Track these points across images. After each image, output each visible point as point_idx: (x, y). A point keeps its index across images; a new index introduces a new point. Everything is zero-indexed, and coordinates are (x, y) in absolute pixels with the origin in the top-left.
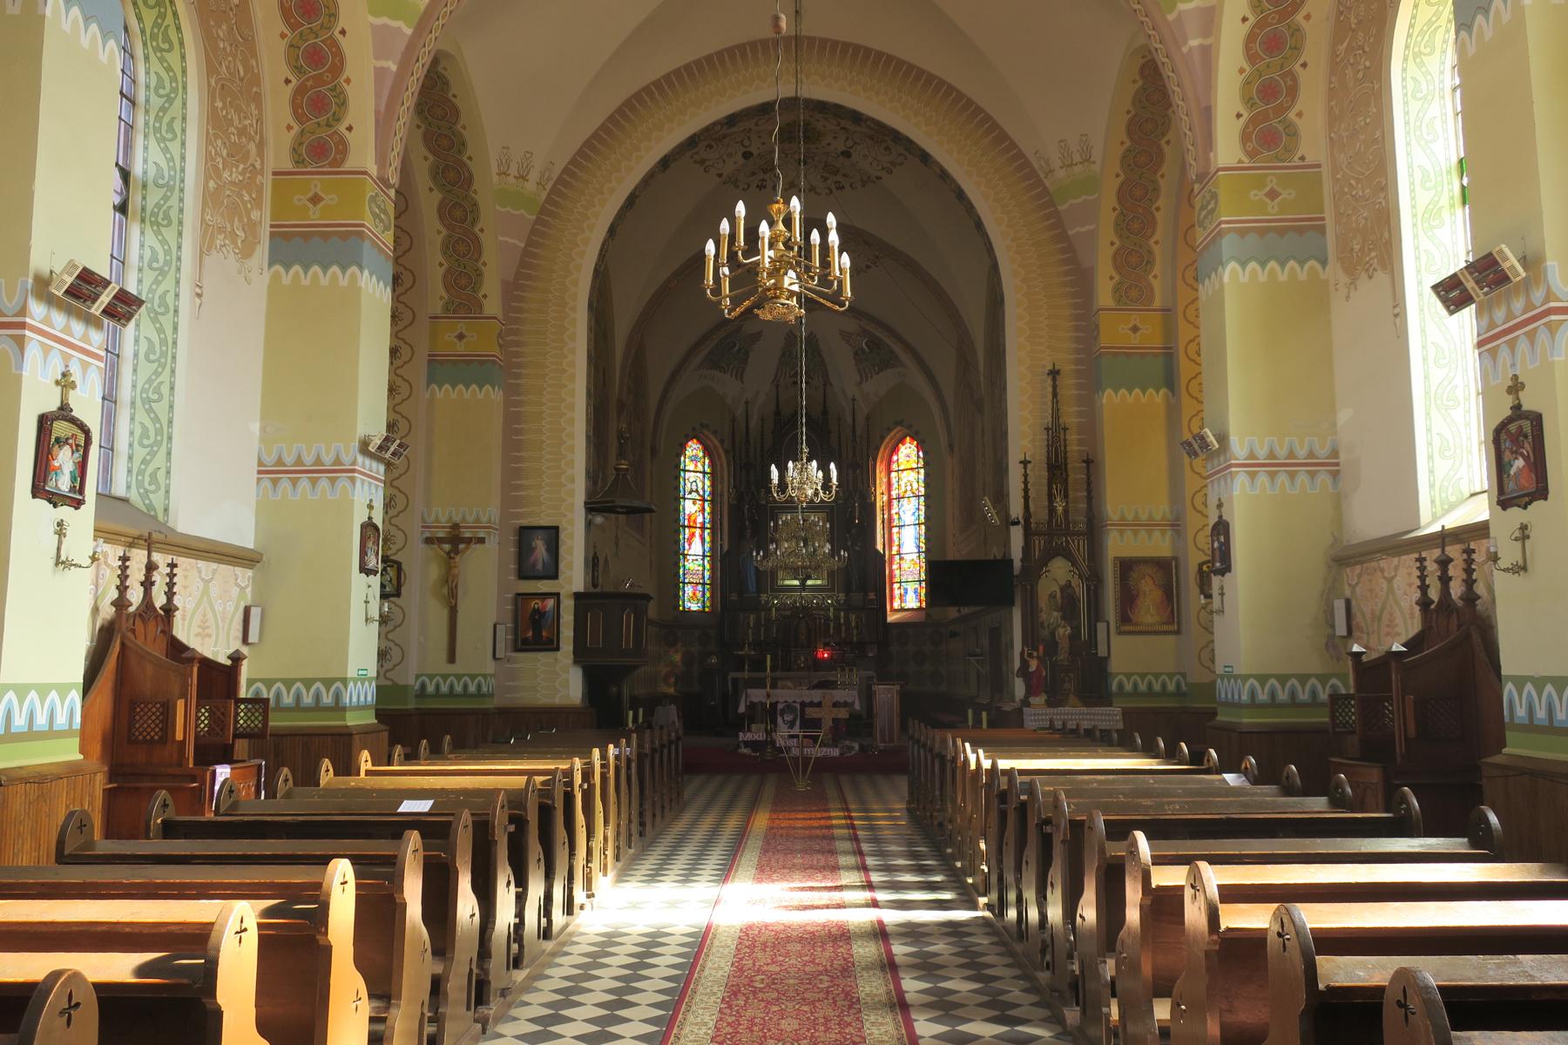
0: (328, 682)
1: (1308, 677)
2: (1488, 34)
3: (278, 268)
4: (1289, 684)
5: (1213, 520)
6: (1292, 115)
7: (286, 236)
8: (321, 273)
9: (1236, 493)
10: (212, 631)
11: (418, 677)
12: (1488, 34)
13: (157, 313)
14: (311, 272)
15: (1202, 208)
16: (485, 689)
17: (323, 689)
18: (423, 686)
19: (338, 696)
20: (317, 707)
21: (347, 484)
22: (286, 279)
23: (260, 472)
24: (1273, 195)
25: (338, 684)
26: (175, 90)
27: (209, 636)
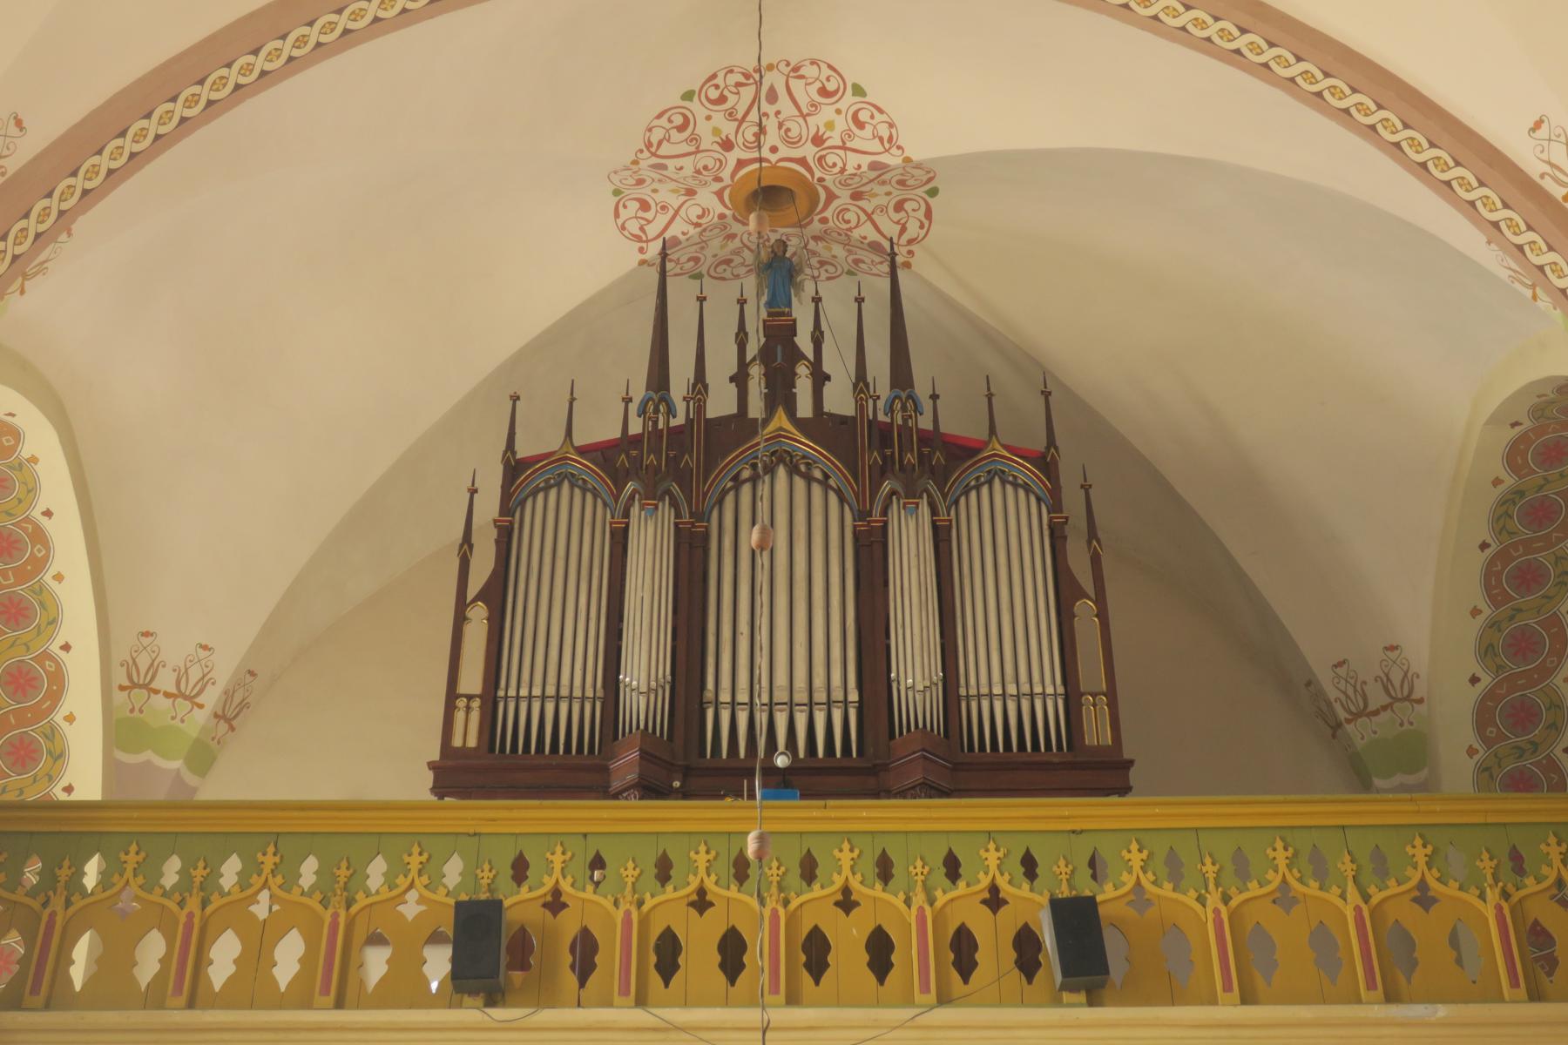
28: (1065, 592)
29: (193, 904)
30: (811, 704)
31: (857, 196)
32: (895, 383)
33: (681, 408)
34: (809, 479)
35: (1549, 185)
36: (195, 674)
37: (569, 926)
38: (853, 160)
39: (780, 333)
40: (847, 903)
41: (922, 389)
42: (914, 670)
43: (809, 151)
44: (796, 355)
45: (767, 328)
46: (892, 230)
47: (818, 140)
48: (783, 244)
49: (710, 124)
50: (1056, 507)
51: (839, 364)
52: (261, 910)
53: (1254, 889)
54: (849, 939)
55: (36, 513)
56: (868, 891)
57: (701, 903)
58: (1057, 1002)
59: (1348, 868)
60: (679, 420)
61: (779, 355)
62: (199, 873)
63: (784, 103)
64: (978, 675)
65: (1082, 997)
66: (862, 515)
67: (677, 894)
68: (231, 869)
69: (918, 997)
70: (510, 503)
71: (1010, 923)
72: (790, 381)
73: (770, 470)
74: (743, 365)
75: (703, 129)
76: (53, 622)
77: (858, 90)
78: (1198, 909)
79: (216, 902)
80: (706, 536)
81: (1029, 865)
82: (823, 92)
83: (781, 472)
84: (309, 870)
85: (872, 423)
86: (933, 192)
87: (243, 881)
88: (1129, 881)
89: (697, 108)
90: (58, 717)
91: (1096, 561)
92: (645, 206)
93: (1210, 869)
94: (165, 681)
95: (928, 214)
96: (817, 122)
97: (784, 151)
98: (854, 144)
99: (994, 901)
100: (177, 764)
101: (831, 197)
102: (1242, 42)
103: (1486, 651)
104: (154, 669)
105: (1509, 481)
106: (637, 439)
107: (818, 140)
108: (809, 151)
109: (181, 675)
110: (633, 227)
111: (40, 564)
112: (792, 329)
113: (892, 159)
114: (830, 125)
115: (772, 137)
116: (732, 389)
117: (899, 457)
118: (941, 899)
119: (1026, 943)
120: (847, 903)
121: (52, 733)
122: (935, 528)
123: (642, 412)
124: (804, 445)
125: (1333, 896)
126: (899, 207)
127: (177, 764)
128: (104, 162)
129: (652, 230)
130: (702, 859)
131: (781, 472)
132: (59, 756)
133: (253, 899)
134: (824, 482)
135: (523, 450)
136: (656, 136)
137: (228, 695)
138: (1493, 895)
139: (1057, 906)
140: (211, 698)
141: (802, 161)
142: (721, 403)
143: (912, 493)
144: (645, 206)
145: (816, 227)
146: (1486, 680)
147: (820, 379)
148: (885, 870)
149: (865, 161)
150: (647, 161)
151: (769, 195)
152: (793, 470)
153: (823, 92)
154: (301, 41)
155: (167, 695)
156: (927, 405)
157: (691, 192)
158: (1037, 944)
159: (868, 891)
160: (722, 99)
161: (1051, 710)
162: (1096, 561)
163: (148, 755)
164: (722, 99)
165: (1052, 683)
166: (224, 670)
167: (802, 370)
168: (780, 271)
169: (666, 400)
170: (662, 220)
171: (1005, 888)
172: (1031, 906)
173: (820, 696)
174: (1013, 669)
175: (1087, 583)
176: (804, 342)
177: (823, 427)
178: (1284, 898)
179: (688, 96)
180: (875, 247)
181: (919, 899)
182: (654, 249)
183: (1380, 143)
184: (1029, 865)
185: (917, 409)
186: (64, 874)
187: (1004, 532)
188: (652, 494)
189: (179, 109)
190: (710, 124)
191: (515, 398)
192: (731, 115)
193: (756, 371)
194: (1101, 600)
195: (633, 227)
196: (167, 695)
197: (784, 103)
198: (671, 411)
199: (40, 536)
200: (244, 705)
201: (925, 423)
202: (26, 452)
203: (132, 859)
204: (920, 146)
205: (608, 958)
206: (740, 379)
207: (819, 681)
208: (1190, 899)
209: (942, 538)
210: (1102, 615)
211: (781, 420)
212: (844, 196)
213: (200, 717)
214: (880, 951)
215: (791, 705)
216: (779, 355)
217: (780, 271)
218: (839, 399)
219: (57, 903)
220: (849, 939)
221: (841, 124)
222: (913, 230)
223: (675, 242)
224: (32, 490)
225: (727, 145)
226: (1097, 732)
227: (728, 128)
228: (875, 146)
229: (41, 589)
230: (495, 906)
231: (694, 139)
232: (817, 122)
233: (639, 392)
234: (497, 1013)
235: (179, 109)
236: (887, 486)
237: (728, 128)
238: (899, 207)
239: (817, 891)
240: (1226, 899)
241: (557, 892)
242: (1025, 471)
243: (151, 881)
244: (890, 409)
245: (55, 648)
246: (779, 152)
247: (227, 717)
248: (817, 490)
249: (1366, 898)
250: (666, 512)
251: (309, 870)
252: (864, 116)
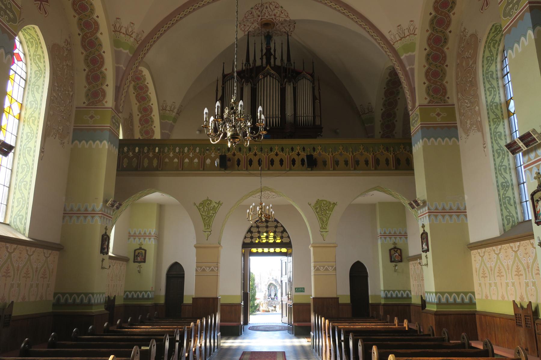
0: (466, 293)
1: (131, 291)
2: (520, 50)
3: (425, 139)
4: (445, 296)
5: (421, 231)
6: (140, 115)
7: (428, 128)
8: (449, 140)
9: (154, 230)
10: (523, 272)
11: (125, 292)
12: (520, 50)
13: (500, 149)
14: (445, 141)
15: (413, 119)
16: (150, 296)
17: (77, 297)
18: (127, 295)
19: (90, 300)
20: (463, 303)
21: (463, 217)
22: (429, 144)
23: (466, 212)
24: (438, 115)
25: (90, 295)
26: (487, 73)
27: (486, 277)
28: (314, 98)
29: (181, 154)
30: (273, 117)
31: (282, 24)
32: (288, 61)
33: (252, 65)
34: (273, 78)
35: (391, 42)
36: (173, 107)
37: (236, 158)
38: (281, 19)
39: (268, 50)
40: (277, 155)
41: (292, 62)
42: (289, 112)
43: (273, 17)
44: (271, 54)
45: (266, 49)
46: (288, 29)
47: (275, 15)
48: (269, 32)
49: (256, 13)
50: (313, 84)
51: (278, 55)
52: (191, 155)
53: (337, 153)
54: (277, 160)
55: (146, 83)
56: (280, 153)
57: (255, 155)
58: (307, 170)
59: (351, 150)
60: (251, 67)
61: (268, 54)
62: (182, 150)
63: (269, 9)
64: (300, 112)
65: (310, 169)
66: (281, 85)
67: (251, 154)
68: (186, 150)
69: (287, 169)
70: (224, 83)
71: (300, 157)
72: (270, 58)
73: (267, 76)
74: (262, 56)
75: (255, 14)
76: (150, 100)
77: (282, 7)
78: (328, 157)
79: (184, 154)
80: (256, 88)
81: (304, 149)
82: (276, 7)
83: (268, 76)
84: (198, 150)
85: (284, 67)
86: (295, 23)
87: (188, 151)
88: (318, 151)
89: (254, 10)
90: (152, 115)
91: (319, 93)
92: (245, 25)
93: (330, 150)
94: (168, 108)
95: (294, 27)
96: (275, 12)
97: (269, 17)
98: (281, 16)
99: (298, 154)
100: (127, 51)
101: (277, 24)
102: (345, 11)
103: (384, 105)
104: (166, 107)
105: (389, 78)
106: (244, 70)
107: (275, 15)
108: (273, 17)
109: (171, 107)
110: (243, 29)
111: (147, 91)
112: (271, 49)
113: (288, 19)
114: (277, 13)
115: (267, 14)
116: (260, 61)
117: (288, 74)
118: (291, 154)
119: (303, 161)
120: (277, 155)
121: (151, 118)
122: (294, 87)
123: (245, 66)
124: (272, 72)
125: (348, 154)
126: (289, 26)
127: (171, 122)
128: (157, 36)
129: (246, 30)
130: (255, 148)
131: (268, 76)
132: (153, 122)
133: (190, 154)
134: (275, 79)
135: (225, 73)
136: (247, 15)
137: (178, 110)
138: (371, 154)
139: (307, 156)
140: (176, 111)
141: (272, 19)
142: (258, 63)
143: (290, 82)
144: (245, 25)
145: (275, 29)
146: (384, 110)
147: (275, 59)
148: (282, 150)
149: (283, 19)
150: (245, 20)
151: (266, 25)
152: (270, 76)
153: (276, 7)
154: (187, 11)
155: (123, 33)
156: (293, 64)
157: (253, 23)
158: (304, 161)
159: (280, 153)
160: (258, 9)
161: (311, 119)
162: (319, 93)
163: (166, 120)
164: (258, 9)
165: (311, 114)
166: (177, 106)
167: (272, 57)
168: (268, 38)
169: (249, 64)
170: (248, 28)
171: (300, 153)
172: (303, 155)
173: (274, 116)
174: (305, 111)
175: (318, 97)
176: (272, 51)
177: (276, 68)
178: (341, 154)
179: (252, 8)
180: (285, 32)
181: (287, 154)
182: (247, 33)
183: (366, 31)
184: (304, 149)
185: (291, 65)
186: (162, 150)
187: (305, 87)
188: (247, 82)
189: (168, 25)
190: (256, 13)
191: (224, 63)
192: (259, 11)
193: (264, 57)
194: (320, 101)
195: (243, 29)
196: (123, 33)
197: (269, 9)
198: (250, 66)
199: (147, 87)
200: (181, 111)
201: (293, 67)
202: (144, 74)
203: (171, 148)
204: (292, 17)
205: (242, 163)
206: (262, 59)
207: (274, 113)
208: (327, 154)
209: (295, 89)
210: (320, 103)
211: (268, 67)
212: (279, 24)
213: (174, 114)
214: (281, 161)
215: (270, 117)
216: (268, 54)
217: (268, 38)
218: (278, 63)
219: (161, 154)
220: (277, 160)
221: (279, 13)
222: (292, 29)
223: (250, 31)
224: (145, 80)
225: (259, 16)
226: (318, 123)
227: (259, 13)
228: (285, 17)
229: (147, 95)
230: (225, 156)
231: (253, 15)
232: (275, 12)
233: (244, 62)
234: (227, 172)
235: (168, 25)
236: (286, 80)
237: (259, 13)
238: (289, 26)
239: (272, 153)
240: (332, 154)
241: (234, 153)
242: (309, 77)
243: (175, 152)
244: (287, 65)
245: (150, 104)
246: (267, 17)
247: (178, 113)
248: (274, 80)
249: (353, 154)
250: (249, 85)
251: (198, 150)
252: (283, 11)
